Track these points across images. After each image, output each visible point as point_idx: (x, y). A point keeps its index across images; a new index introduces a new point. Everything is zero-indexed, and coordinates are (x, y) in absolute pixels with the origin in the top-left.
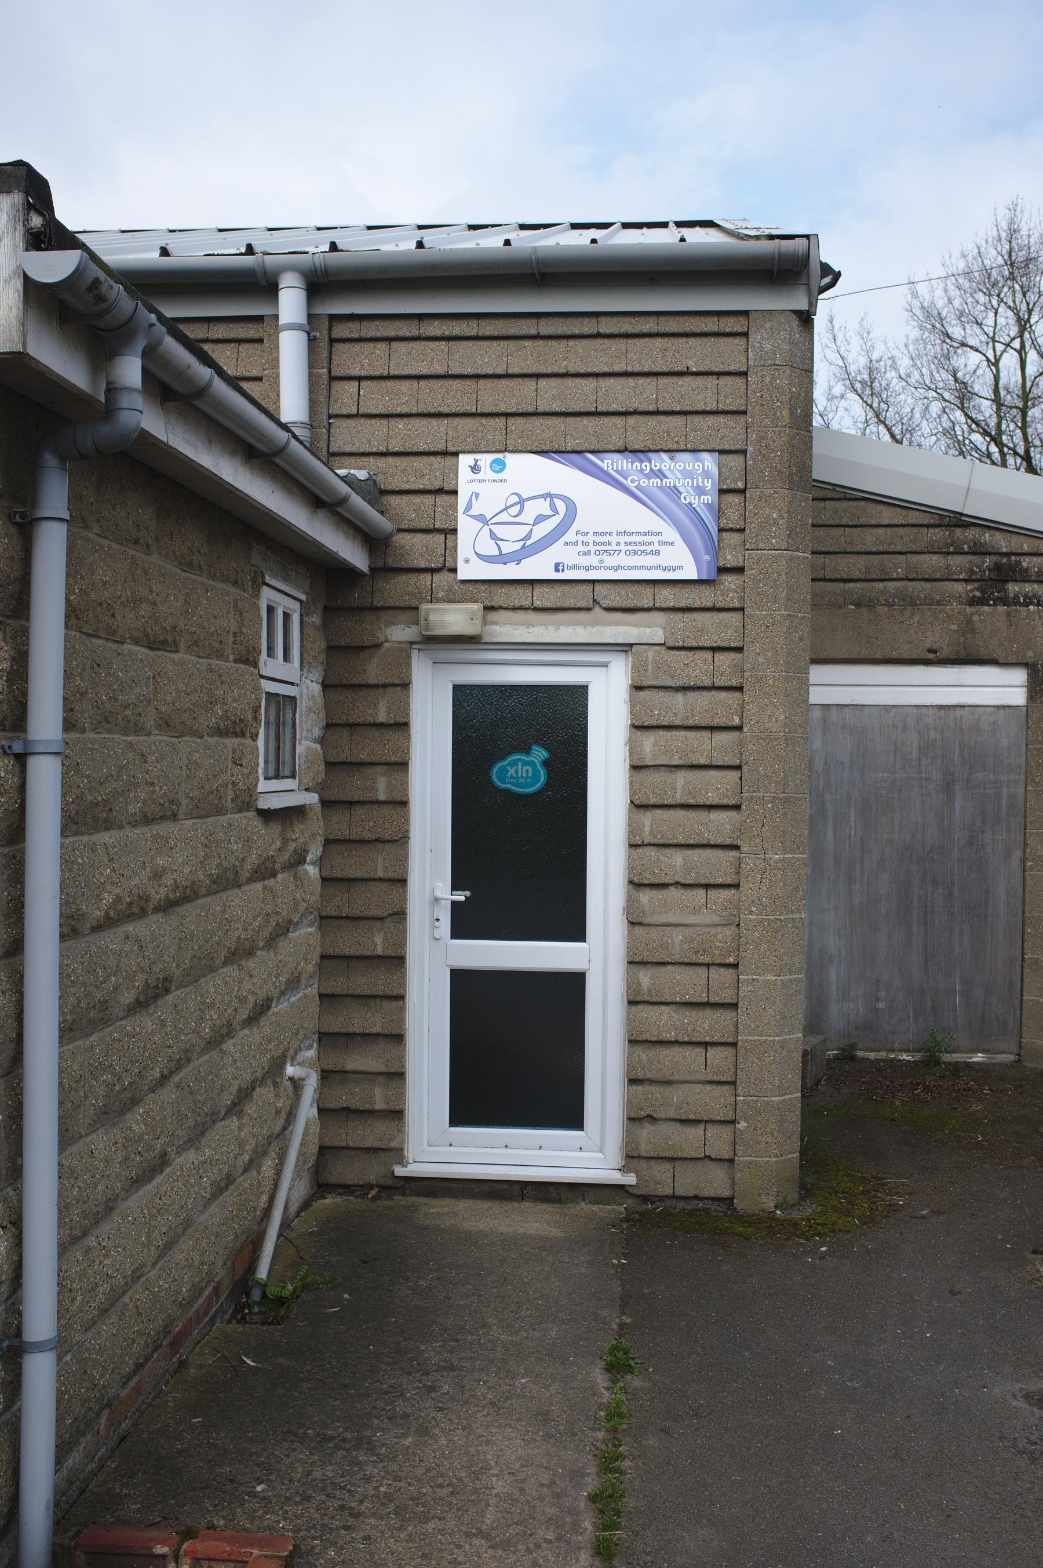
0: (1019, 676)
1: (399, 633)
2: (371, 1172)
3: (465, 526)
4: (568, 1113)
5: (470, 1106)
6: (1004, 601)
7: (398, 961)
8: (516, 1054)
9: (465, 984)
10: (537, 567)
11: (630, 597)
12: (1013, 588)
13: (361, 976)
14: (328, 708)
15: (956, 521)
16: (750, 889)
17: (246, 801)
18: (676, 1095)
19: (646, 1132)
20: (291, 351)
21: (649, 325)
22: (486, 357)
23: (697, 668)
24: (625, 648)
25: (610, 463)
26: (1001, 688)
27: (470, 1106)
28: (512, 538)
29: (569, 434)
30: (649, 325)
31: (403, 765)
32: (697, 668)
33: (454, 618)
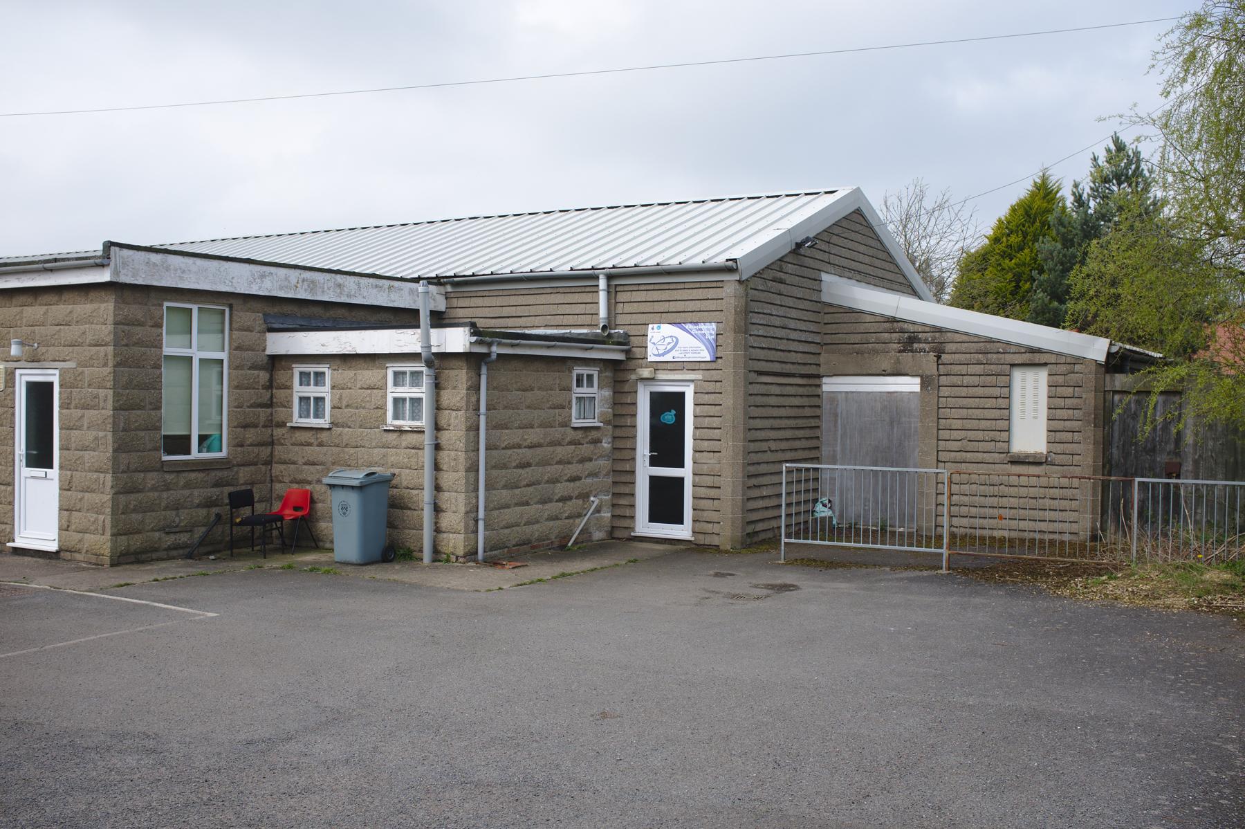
0: (918, 380)
1: (633, 377)
2: (624, 534)
3: (650, 346)
4: (679, 520)
5: (654, 518)
6: (912, 351)
7: (633, 472)
8: (667, 501)
9: (654, 481)
10: (668, 358)
11: (693, 366)
12: (915, 346)
13: (623, 477)
14: (614, 398)
15: (894, 320)
16: (724, 452)
17: (566, 424)
18: (705, 514)
19: (697, 524)
20: (602, 297)
21: (698, 285)
22: (656, 295)
23: (711, 387)
24: (692, 381)
25: (688, 326)
26: (909, 385)
27: (654, 518)
28: (662, 349)
29: (678, 318)
30: (698, 285)
31: (634, 415)
32: (711, 387)
33: (646, 373)
